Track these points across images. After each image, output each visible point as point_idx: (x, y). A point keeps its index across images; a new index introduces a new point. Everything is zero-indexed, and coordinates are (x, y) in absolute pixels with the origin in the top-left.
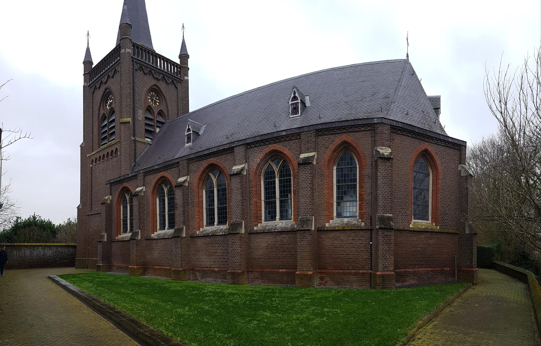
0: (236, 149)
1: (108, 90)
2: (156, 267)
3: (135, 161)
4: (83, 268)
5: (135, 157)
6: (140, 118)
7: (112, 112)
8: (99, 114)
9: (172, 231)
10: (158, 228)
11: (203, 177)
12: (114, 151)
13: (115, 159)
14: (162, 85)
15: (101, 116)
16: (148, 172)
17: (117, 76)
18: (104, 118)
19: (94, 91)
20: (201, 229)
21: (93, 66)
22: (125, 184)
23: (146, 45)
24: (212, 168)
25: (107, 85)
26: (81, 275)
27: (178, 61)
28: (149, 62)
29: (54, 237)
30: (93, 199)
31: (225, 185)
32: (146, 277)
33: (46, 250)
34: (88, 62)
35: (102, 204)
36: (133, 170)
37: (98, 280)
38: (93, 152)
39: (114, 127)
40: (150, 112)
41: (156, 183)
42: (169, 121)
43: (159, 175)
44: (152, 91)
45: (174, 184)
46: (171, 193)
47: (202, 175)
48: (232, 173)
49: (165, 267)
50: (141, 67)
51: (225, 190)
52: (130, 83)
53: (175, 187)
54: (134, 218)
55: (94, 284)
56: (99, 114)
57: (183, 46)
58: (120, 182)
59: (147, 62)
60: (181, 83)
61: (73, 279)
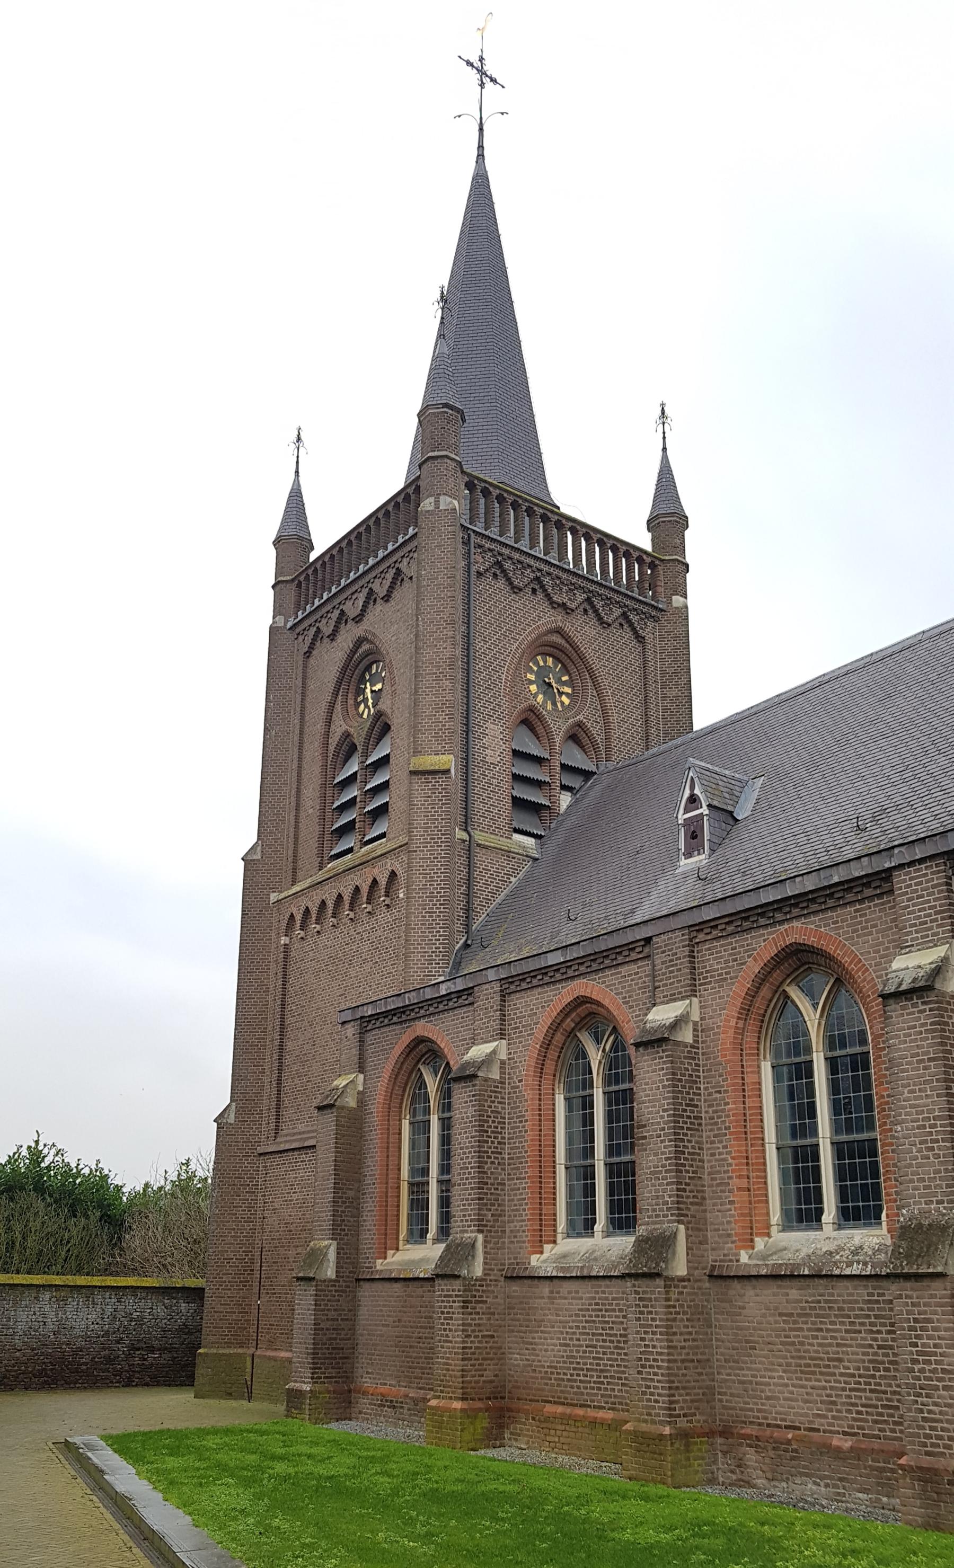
0: (900, 879)
1: (365, 647)
2: (549, 1408)
3: (468, 926)
4: (229, 1395)
5: (468, 910)
6: (492, 756)
7: (381, 727)
8: (327, 735)
9: (624, 1243)
10: (562, 1225)
11: (759, 1003)
12: (383, 882)
13: (384, 916)
14: (584, 632)
15: (334, 741)
16: (516, 982)
17: (405, 593)
18: (348, 749)
19: (312, 647)
20: (760, 1243)
21: (313, 556)
22: (422, 1028)
23: (521, 485)
24: (800, 961)
25: (365, 625)
26: (211, 1442)
27: (644, 541)
28: (533, 543)
29: (116, 1242)
30: (287, 1084)
31: (863, 1042)
32: (501, 1453)
33: (72, 1304)
34: (292, 537)
35: (320, 1108)
36: (457, 965)
37: (281, 1468)
38: (294, 883)
39: (385, 786)
40: (532, 729)
41: (555, 1027)
42: (611, 765)
43: (567, 992)
44: (544, 654)
45: (631, 1034)
46: (619, 1069)
47: (752, 994)
48: (891, 988)
49: (591, 1413)
50: (498, 563)
51: (861, 1062)
52: (453, 623)
53: (637, 1045)
54: (456, 1179)
55: (259, 1497)
56: (327, 735)
57: (666, 482)
58: (400, 1014)
59: (524, 545)
60: (656, 619)
61: (172, 1462)
